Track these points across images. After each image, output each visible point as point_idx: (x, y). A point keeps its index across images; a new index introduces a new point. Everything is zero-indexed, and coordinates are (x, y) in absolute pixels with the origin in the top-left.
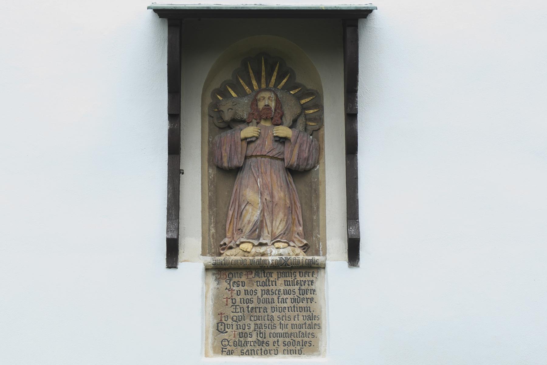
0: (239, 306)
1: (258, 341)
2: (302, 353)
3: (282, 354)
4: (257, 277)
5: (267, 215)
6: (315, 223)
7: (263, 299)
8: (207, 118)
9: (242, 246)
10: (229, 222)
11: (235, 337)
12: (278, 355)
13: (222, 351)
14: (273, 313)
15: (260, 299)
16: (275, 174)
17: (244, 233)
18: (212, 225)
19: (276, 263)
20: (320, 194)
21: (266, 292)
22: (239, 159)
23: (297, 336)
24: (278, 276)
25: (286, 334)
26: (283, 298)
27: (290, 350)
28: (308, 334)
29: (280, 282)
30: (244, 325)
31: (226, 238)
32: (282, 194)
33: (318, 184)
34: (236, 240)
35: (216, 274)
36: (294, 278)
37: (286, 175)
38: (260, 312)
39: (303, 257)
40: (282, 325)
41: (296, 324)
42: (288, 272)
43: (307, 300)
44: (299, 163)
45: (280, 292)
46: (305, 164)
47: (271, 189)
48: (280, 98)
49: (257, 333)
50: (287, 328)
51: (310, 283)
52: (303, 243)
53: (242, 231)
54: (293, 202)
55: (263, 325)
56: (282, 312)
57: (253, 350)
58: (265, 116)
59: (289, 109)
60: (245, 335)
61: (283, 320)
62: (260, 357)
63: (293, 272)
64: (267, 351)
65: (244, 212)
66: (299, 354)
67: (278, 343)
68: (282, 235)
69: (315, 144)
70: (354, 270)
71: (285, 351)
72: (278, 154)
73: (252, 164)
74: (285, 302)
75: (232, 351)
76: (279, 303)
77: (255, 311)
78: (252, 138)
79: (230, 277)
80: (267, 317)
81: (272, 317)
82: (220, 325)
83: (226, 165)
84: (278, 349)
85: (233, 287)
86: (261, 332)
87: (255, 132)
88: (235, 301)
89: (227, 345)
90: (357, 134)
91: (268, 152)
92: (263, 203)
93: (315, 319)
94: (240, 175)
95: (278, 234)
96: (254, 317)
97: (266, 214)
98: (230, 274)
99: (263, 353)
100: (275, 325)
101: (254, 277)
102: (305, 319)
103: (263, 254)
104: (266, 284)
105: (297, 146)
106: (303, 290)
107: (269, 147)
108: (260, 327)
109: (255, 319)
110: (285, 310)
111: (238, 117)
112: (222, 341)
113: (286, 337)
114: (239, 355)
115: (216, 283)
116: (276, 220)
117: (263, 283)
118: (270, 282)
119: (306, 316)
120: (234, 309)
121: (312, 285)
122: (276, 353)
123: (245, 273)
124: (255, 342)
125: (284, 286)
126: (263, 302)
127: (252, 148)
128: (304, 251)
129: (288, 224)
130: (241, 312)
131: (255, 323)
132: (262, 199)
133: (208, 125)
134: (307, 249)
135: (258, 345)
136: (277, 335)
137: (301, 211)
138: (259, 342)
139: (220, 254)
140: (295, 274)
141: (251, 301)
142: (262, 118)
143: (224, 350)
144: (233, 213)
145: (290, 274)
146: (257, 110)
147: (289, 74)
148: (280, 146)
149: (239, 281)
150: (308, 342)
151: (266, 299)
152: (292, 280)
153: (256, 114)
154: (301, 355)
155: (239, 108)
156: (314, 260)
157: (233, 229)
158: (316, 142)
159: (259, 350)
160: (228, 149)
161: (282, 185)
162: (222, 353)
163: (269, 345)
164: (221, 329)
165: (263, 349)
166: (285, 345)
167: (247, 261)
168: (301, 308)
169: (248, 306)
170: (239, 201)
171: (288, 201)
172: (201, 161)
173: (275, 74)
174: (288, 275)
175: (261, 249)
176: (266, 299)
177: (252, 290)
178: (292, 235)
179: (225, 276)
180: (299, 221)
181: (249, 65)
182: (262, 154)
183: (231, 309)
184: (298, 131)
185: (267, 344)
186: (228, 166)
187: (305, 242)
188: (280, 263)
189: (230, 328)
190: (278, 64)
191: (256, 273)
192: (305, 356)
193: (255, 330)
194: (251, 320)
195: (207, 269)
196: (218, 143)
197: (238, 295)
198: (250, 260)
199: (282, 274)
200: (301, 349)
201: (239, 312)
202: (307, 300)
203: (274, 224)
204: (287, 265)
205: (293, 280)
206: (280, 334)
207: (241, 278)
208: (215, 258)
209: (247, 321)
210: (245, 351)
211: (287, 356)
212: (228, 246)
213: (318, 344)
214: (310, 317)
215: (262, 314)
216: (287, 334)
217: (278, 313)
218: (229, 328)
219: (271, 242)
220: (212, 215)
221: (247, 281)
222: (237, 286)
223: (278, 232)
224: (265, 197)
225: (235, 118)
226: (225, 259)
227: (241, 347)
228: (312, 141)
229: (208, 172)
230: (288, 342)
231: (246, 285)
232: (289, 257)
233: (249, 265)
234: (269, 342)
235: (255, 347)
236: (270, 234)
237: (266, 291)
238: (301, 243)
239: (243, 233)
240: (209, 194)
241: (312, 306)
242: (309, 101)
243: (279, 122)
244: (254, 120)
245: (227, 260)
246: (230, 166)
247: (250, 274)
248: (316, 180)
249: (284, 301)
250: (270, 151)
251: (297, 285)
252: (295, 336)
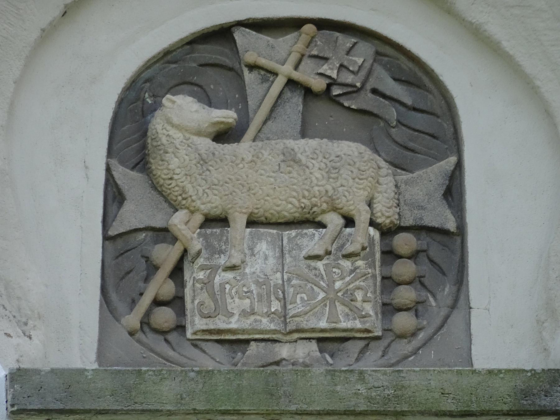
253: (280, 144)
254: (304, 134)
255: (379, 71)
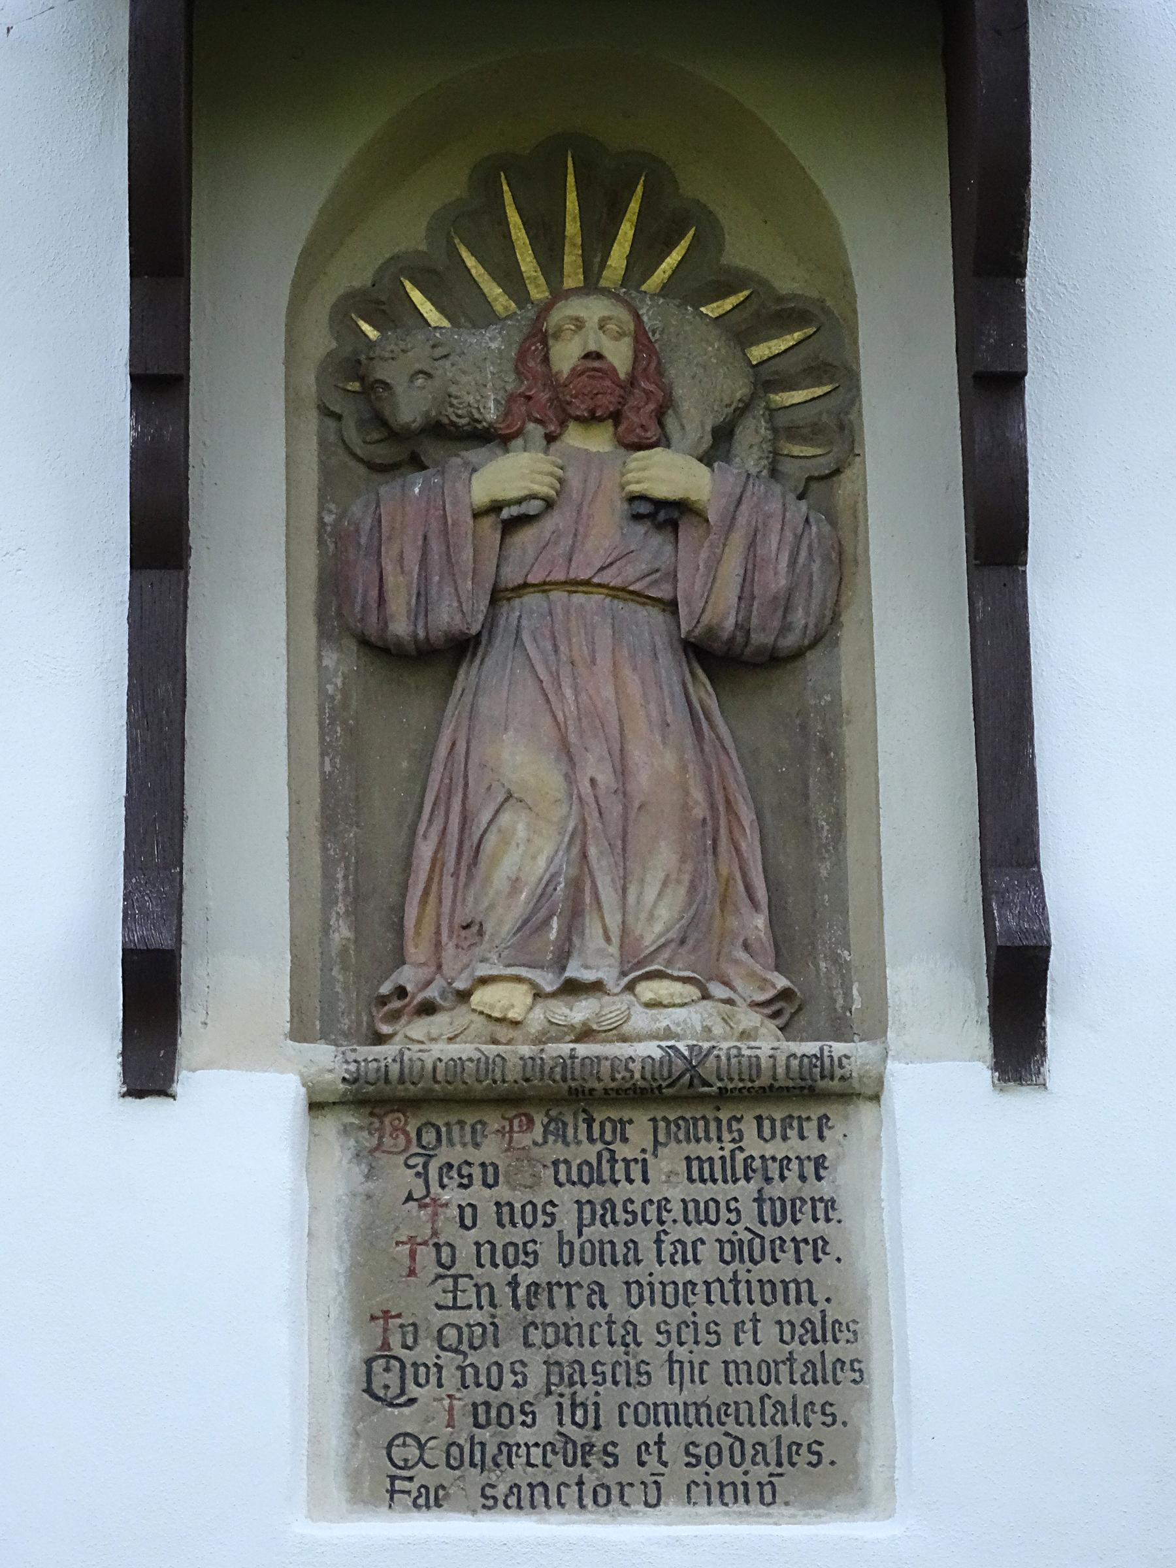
0: (471, 1277)
1: (566, 1443)
2: (777, 1500)
3: (684, 1505)
4: (555, 1141)
5: (602, 853)
6: (826, 897)
7: (588, 1245)
8: (311, 422)
9: (480, 998)
10: (419, 893)
11: (453, 1427)
12: (662, 1506)
13: (392, 1492)
14: (633, 1311)
15: (571, 1244)
16: (635, 669)
17: (491, 940)
18: (341, 908)
19: (648, 1076)
20: (847, 762)
21: (600, 1212)
22: (463, 599)
23: (750, 1416)
24: (655, 1136)
25: (698, 1410)
26: (679, 1241)
27: (720, 1483)
28: (806, 1407)
29: (665, 1165)
30: (494, 1369)
31: (406, 967)
32: (669, 761)
33: (834, 716)
34: (453, 974)
35: (361, 1128)
36: (732, 1146)
37: (688, 676)
38: (570, 1304)
39: (776, 1044)
40: (676, 1366)
41: (746, 1362)
42: (704, 1118)
43: (797, 1250)
44: (748, 618)
45: (664, 1214)
46: (776, 624)
47: (618, 735)
48: (654, 333)
49: (560, 1405)
50: (703, 1382)
51: (809, 1168)
52: (774, 986)
53: (481, 933)
54: (720, 797)
55: (588, 1369)
56: (676, 1304)
57: (542, 1484)
58: (583, 407)
59: (693, 377)
60: (499, 1415)
61: (681, 1344)
62: (574, 1517)
63: (730, 1116)
64: (608, 1489)
65: (492, 839)
66: (762, 1502)
67: (660, 1451)
68: (673, 945)
69: (820, 534)
70: (1021, 1100)
71: (693, 1486)
72: (648, 579)
73: (524, 622)
74: (690, 1256)
75: (441, 1493)
76: (661, 1263)
77: (546, 1303)
78: (524, 505)
79: (424, 1143)
80: (604, 1327)
81: (630, 1328)
82: (378, 1366)
83: (400, 627)
84: (659, 1479)
85: (440, 1190)
86: (578, 1400)
87: (539, 477)
88: (454, 1255)
89: (417, 1463)
90: (1025, 472)
91: (602, 569)
92: (580, 797)
93: (838, 1335)
94: (466, 677)
95: (654, 942)
96: (545, 1331)
97: (592, 851)
98: (424, 1131)
99: (588, 1501)
100: (643, 1368)
101: (540, 1140)
102: (787, 1337)
103: (585, 1034)
104: (600, 1176)
105: (738, 539)
106: (778, 1204)
107: (607, 543)
108: (571, 1376)
109: (550, 1339)
110: (694, 1294)
111: (459, 416)
112: (390, 1446)
113: (701, 1424)
114: (474, 1512)
115: (358, 1171)
116: (642, 881)
117: (585, 1168)
118: (620, 1166)
119: (792, 1325)
120: (445, 1292)
121: (819, 1178)
122: (652, 1500)
123: (496, 1126)
124: (549, 1448)
125: (686, 1181)
126: (588, 1259)
127: (524, 550)
128: (781, 1021)
129: (699, 898)
130: (480, 1307)
131: (549, 1356)
132: (576, 781)
133: (319, 456)
134: (793, 1015)
135: (566, 1463)
136: (656, 1415)
137: (757, 843)
138: (570, 1446)
139: (380, 1039)
140: (735, 1126)
141: (526, 1254)
142: (570, 416)
143: (399, 1485)
144: (436, 852)
145: (713, 1126)
146: (550, 379)
147: (694, 229)
148: (657, 540)
149: (470, 1160)
150: (805, 1444)
151: (601, 1242)
152: (721, 1153)
153: (544, 396)
154: (773, 1509)
155: (464, 372)
156: (827, 1061)
157: (438, 927)
158: (827, 528)
159: (567, 1486)
160: (413, 558)
161: (669, 719)
162: (392, 1498)
163: (616, 1463)
164: (387, 1387)
165: (590, 1480)
166: (693, 1461)
167: (509, 1064)
168: (768, 1287)
169: (516, 1275)
170: (465, 797)
171: (698, 794)
172: (284, 607)
173: (627, 230)
174: (701, 1134)
175: (571, 1010)
176: (601, 1242)
177: (530, 1202)
178: (719, 954)
179: (402, 1137)
180: (748, 888)
181: (505, 188)
182: (572, 576)
183: (431, 1290)
184: (739, 474)
185: (611, 1457)
186: (415, 635)
187: (782, 982)
188: (666, 1074)
189: (428, 1382)
190: (640, 189)
191: (549, 1123)
192: (791, 1510)
193: (549, 1393)
194: (527, 1344)
195: (316, 1106)
196: (368, 527)
197: (463, 1225)
198: (521, 1058)
199: (673, 1128)
200: (772, 1479)
201: (469, 1307)
202: (797, 1250)
203: (631, 899)
204: (696, 1081)
205: (727, 1153)
206: (672, 1408)
207: (477, 1145)
208: (354, 1050)
209: (512, 1350)
210: (502, 1489)
211: (703, 1510)
212: (415, 1002)
213: (855, 1454)
214: (814, 1330)
215: (583, 1314)
216: (703, 1410)
217: (658, 1312)
218: (422, 1380)
219: (619, 979)
220: (339, 861)
221: (507, 1161)
222: (461, 1185)
223: (651, 934)
224: (590, 773)
225: (446, 421)
226: (402, 1053)
227: (482, 1471)
228: (807, 521)
229: (319, 667)
230: (708, 1449)
231: (501, 1179)
232: (706, 1045)
233: (516, 1082)
234: (615, 1445)
235: (549, 1470)
236: (615, 940)
237: (598, 1207)
238: (762, 989)
239: (486, 937)
240: (322, 763)
241: (824, 1275)
242: (785, 351)
243: (649, 434)
244: (531, 426)
245: (410, 1060)
246: (421, 634)
247: (520, 1126)
248: (828, 698)
249: (684, 1253)
250: (611, 564)
251: (748, 1179)
252: (743, 1417)
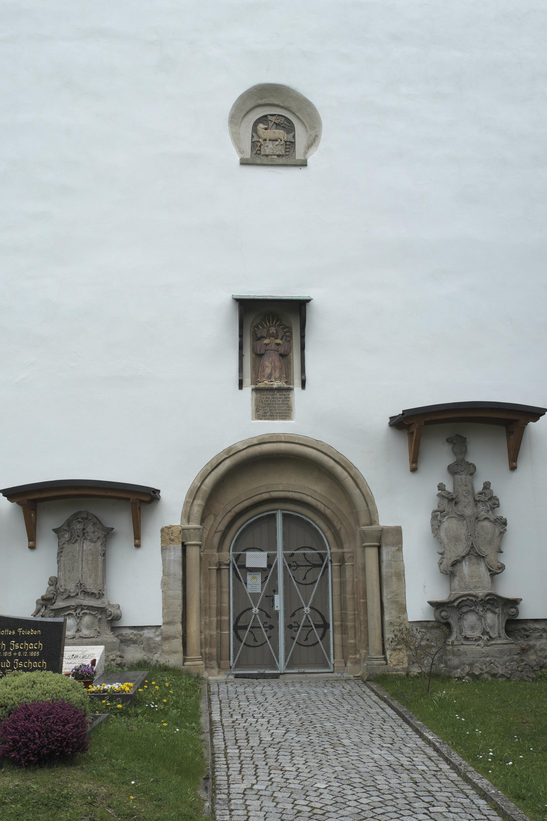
70: (304, 391)
83: (258, 353)
94: (263, 356)
103: (272, 385)
173: (275, 320)
185: (274, 416)
195: (253, 390)
241: (289, 403)
253: (273, 130)
254: (276, 129)
255: (285, 121)
